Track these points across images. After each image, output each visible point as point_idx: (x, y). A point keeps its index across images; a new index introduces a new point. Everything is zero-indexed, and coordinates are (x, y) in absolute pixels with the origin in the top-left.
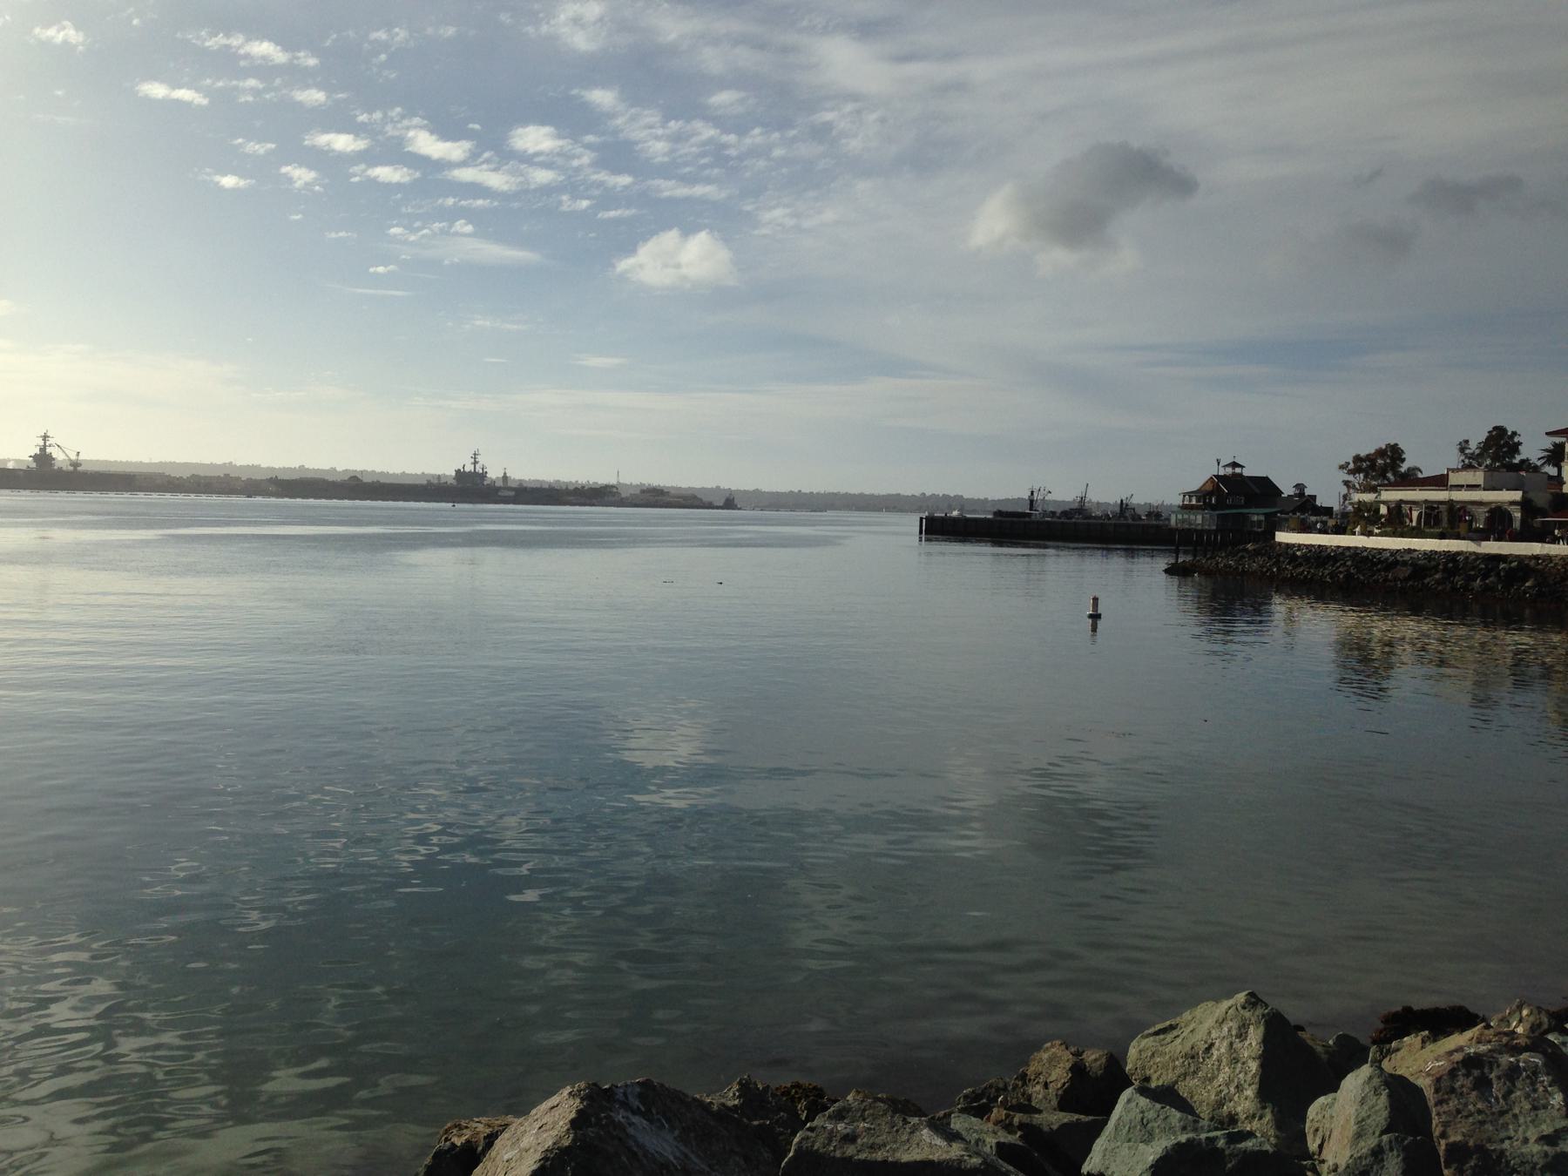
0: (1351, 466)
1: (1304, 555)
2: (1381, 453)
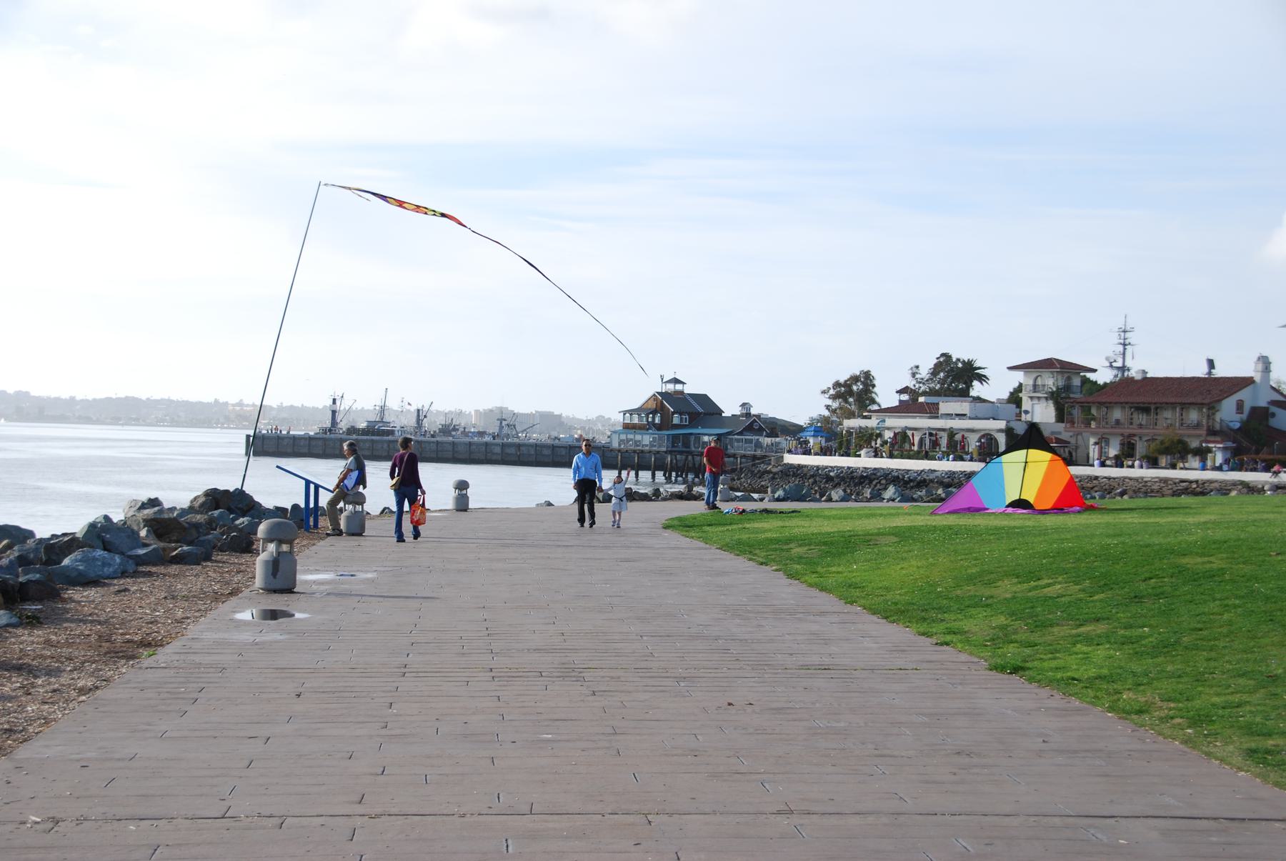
0: (832, 392)
1: (838, 476)
2: (855, 379)
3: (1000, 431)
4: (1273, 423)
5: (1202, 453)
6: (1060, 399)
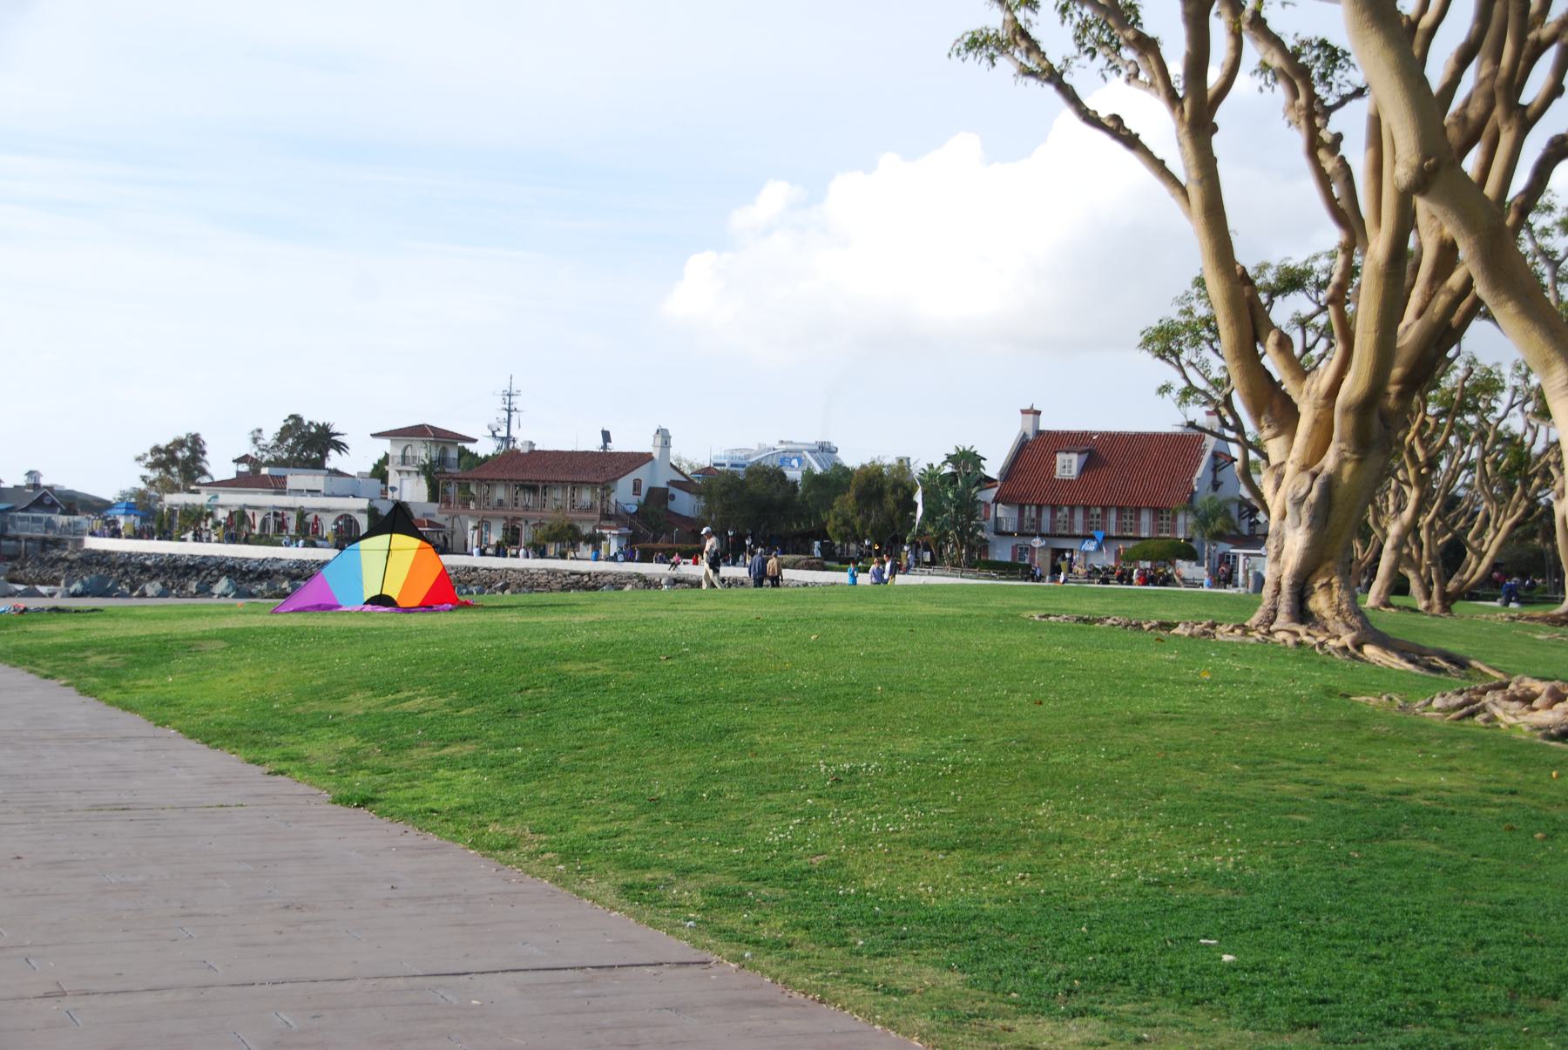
2: (180, 444)
3: (361, 511)
4: (673, 506)
5: (595, 541)
6: (434, 475)
